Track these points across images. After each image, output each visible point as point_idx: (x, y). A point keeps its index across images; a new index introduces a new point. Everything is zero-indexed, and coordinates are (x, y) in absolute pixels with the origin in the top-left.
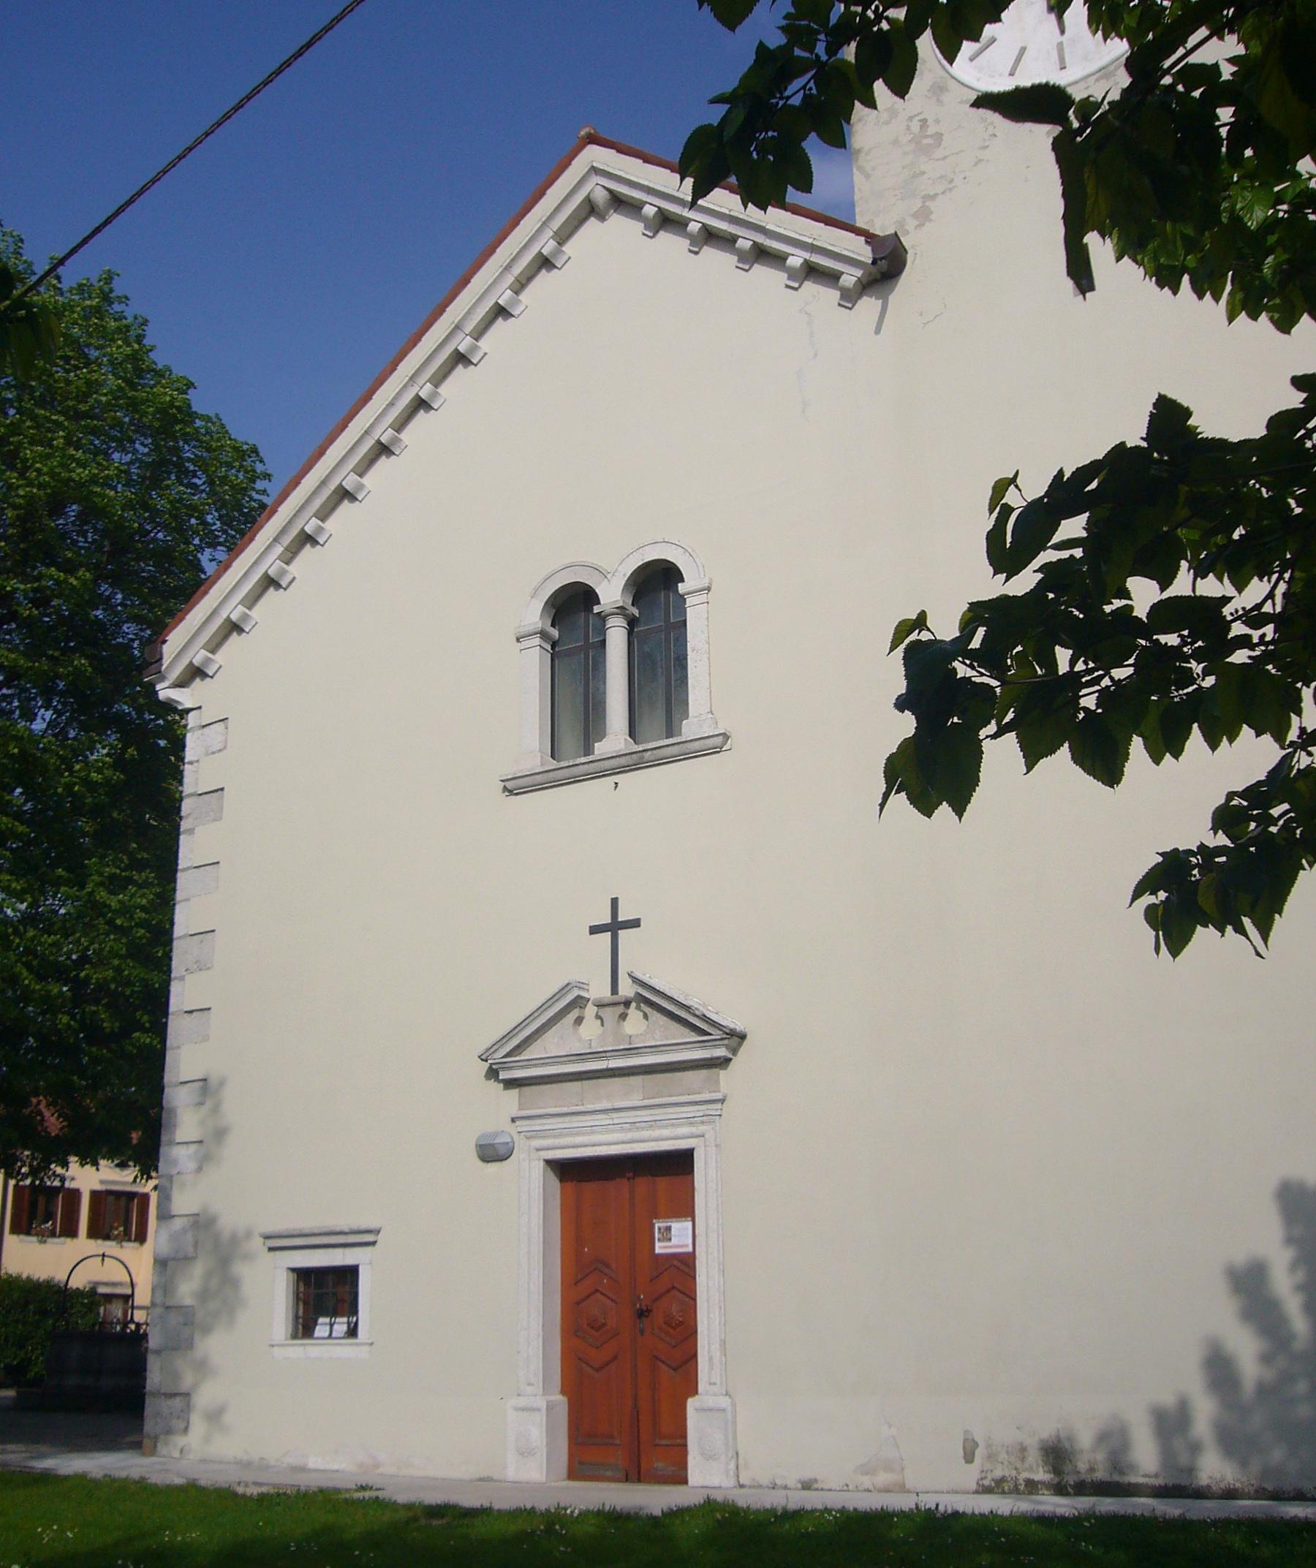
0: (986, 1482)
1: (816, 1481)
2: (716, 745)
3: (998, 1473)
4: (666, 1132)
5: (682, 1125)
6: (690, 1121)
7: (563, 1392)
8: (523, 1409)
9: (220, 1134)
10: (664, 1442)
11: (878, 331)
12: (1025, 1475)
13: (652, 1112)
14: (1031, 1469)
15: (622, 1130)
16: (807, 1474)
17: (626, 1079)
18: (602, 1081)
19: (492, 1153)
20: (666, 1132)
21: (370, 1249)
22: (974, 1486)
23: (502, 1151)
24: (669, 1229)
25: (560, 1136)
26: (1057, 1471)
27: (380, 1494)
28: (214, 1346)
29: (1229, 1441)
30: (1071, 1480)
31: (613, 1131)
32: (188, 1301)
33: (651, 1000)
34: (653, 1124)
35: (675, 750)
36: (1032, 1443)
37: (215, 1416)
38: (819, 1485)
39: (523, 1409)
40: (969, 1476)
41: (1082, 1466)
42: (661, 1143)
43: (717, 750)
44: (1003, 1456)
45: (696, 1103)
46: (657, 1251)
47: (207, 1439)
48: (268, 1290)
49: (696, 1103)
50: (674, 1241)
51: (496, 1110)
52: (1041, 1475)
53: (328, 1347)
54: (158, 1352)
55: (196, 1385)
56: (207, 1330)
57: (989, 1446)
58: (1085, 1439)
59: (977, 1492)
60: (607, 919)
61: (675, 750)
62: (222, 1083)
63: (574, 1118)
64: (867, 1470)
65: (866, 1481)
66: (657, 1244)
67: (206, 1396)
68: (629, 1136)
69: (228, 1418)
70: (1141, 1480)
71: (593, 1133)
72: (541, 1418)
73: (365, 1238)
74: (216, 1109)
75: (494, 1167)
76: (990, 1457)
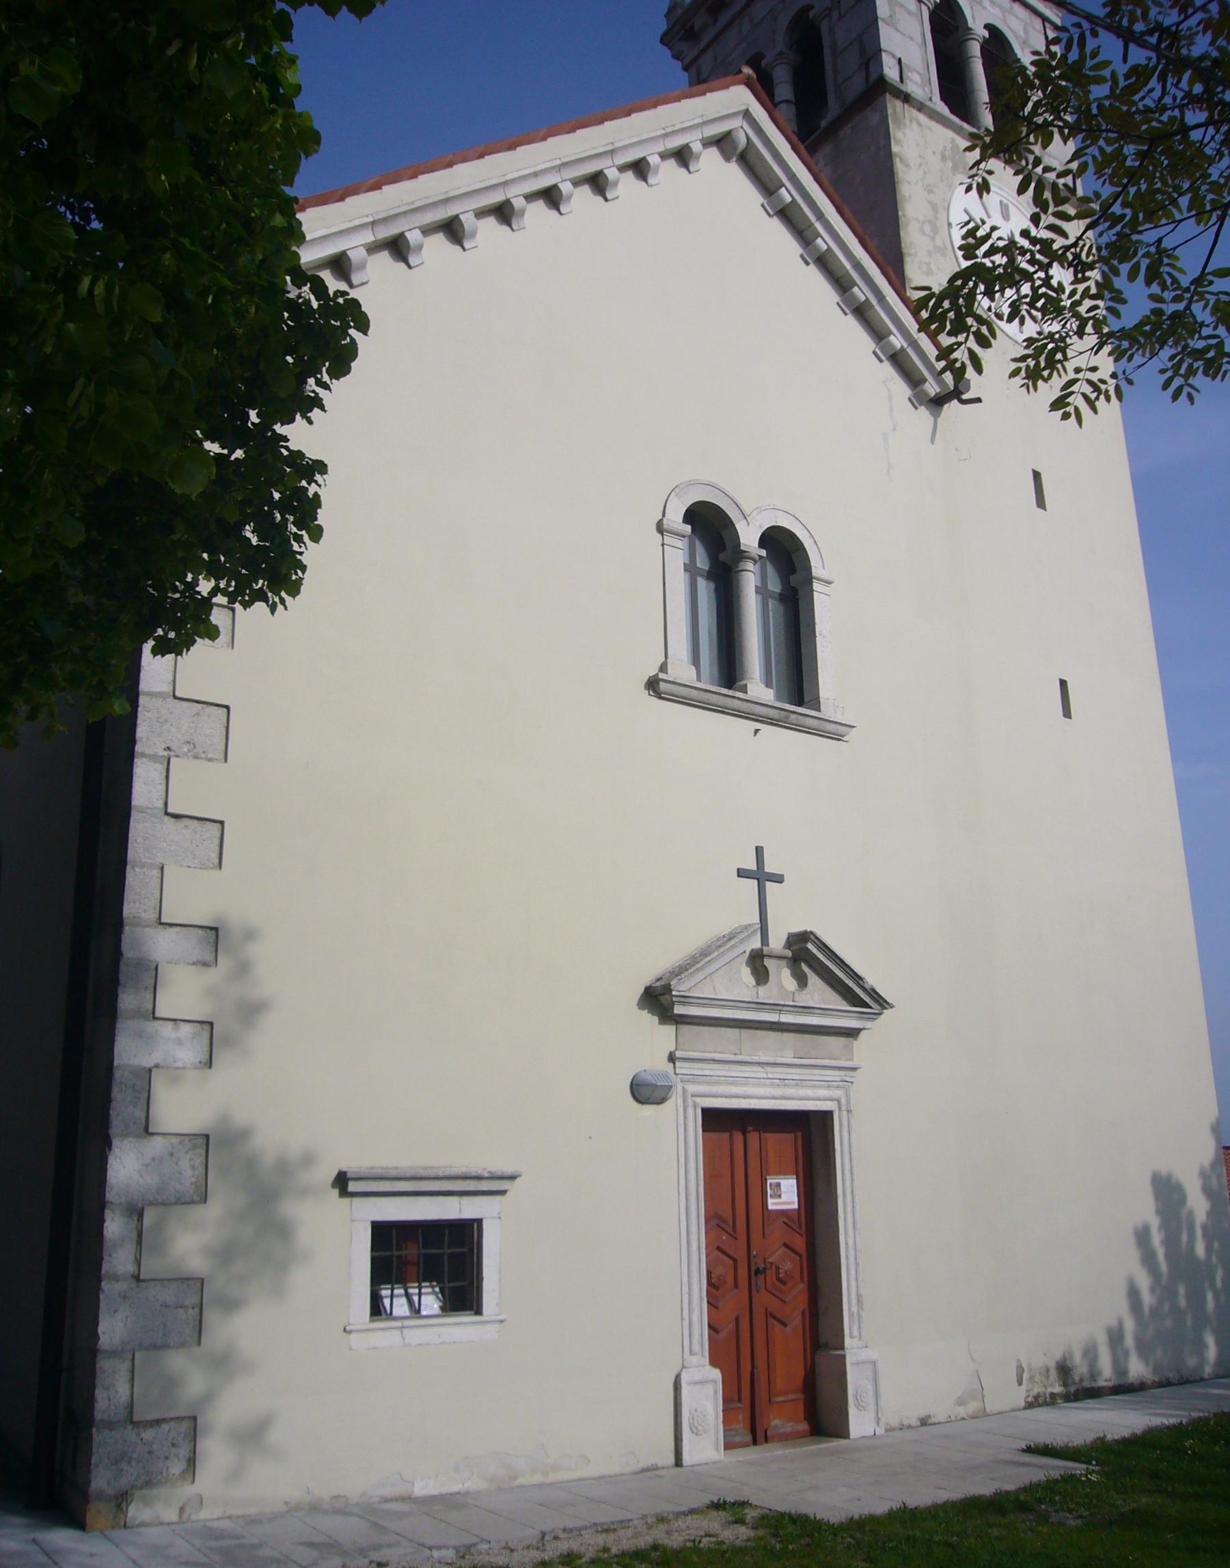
0: (1030, 1399)
1: (929, 1416)
2: (834, 733)
3: (1035, 1391)
4: (809, 1092)
5: (821, 1087)
6: (828, 1085)
7: (714, 1362)
8: (696, 1383)
9: (251, 1012)
10: (781, 1399)
11: (932, 441)
12: (1050, 1390)
13: (842, 1073)
14: (1052, 1385)
15: (772, 1085)
16: (922, 1413)
17: (779, 1034)
18: (758, 1032)
19: (645, 1092)
20: (809, 1092)
21: (498, 1198)
22: (1023, 1404)
23: (658, 1094)
24: (778, 1185)
25: (717, 1083)
26: (1065, 1384)
27: (243, 1541)
28: (247, 1328)
29: (1143, 1349)
30: (1072, 1389)
31: (764, 1085)
32: (196, 1264)
33: (805, 953)
34: (799, 1083)
35: (814, 723)
36: (1052, 1364)
37: (252, 1437)
38: (933, 1420)
39: (696, 1383)
40: (1019, 1396)
41: (1077, 1378)
42: (734, 1100)
43: (838, 737)
44: (1038, 1377)
45: (839, 1068)
46: (770, 1207)
47: (236, 1474)
48: (338, 1242)
49: (839, 1068)
50: (784, 1198)
51: (652, 1043)
52: (1058, 1389)
53: (424, 1327)
54: (125, 1352)
55: (209, 1398)
56: (230, 1305)
57: (1030, 1370)
58: (1077, 1359)
59: (1025, 1408)
60: (769, 868)
61: (814, 723)
62: (250, 935)
63: (733, 1067)
64: (961, 1402)
65: (962, 1411)
66: (770, 1201)
67: (232, 1407)
68: (778, 1092)
69: (275, 1436)
70: (1104, 1384)
71: (746, 1084)
72: (709, 1389)
73: (494, 1184)
74: (243, 969)
75: (648, 1110)
76: (1031, 1378)
